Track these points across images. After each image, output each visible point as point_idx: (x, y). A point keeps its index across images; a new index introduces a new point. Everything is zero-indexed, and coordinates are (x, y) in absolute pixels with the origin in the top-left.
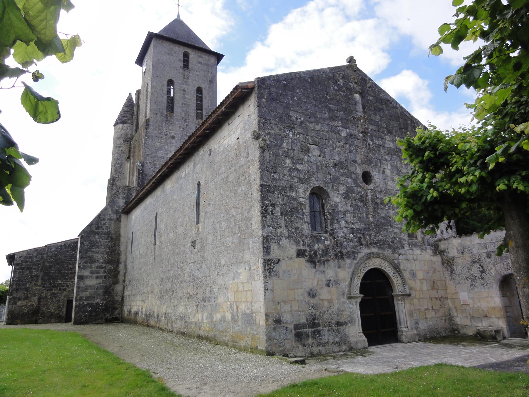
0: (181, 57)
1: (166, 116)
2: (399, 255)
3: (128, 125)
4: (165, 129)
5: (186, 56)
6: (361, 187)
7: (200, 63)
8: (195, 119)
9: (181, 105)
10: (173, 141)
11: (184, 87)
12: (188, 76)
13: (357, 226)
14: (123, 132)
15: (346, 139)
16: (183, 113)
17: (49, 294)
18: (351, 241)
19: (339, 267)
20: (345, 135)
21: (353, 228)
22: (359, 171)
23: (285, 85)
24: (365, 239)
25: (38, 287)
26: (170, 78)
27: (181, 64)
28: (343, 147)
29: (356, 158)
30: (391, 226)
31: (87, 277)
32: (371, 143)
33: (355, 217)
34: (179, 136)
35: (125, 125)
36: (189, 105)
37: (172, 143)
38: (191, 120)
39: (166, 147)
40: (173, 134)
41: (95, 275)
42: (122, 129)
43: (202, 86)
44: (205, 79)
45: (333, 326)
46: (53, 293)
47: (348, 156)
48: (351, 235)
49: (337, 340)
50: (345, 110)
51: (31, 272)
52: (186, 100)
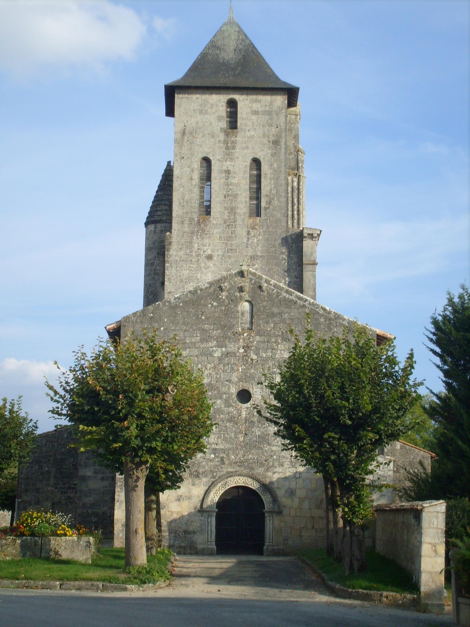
0: (223, 110)
1: (199, 222)
2: (274, 473)
3: (163, 225)
4: (196, 245)
5: (232, 104)
6: (233, 406)
7: (256, 113)
8: (247, 219)
9: (222, 198)
10: (210, 264)
11: (228, 164)
12: (234, 142)
13: (221, 447)
14: (155, 238)
15: (220, 359)
16: (226, 212)
17: (63, 498)
18: (211, 460)
19: (193, 485)
20: (220, 355)
21: (216, 449)
22: (234, 390)
23: (151, 318)
24: (229, 459)
25: (50, 488)
26: (204, 155)
27: (224, 124)
28: (215, 368)
29: (230, 377)
30: (269, 444)
31: (89, 477)
32: (255, 357)
33: (220, 438)
34: (220, 253)
35: (159, 226)
36: (236, 196)
37: (209, 267)
38: (239, 222)
39: (199, 276)
40: (209, 252)
41: (99, 476)
42: (155, 232)
43: (260, 156)
44: (265, 141)
45: (181, 534)
46: (69, 498)
47: (220, 377)
48: (213, 456)
49: (183, 544)
50: (223, 327)
51: (41, 467)
52: (230, 187)
